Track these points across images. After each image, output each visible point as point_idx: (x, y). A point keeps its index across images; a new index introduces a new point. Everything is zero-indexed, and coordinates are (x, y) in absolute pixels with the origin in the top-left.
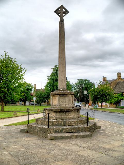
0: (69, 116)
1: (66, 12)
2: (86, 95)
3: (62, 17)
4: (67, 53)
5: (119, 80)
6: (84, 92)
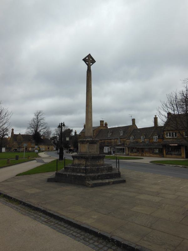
0: (99, 163)
1: (93, 61)
2: (68, 141)
3: (89, 66)
4: (94, 99)
5: (102, 128)
6: (67, 138)
